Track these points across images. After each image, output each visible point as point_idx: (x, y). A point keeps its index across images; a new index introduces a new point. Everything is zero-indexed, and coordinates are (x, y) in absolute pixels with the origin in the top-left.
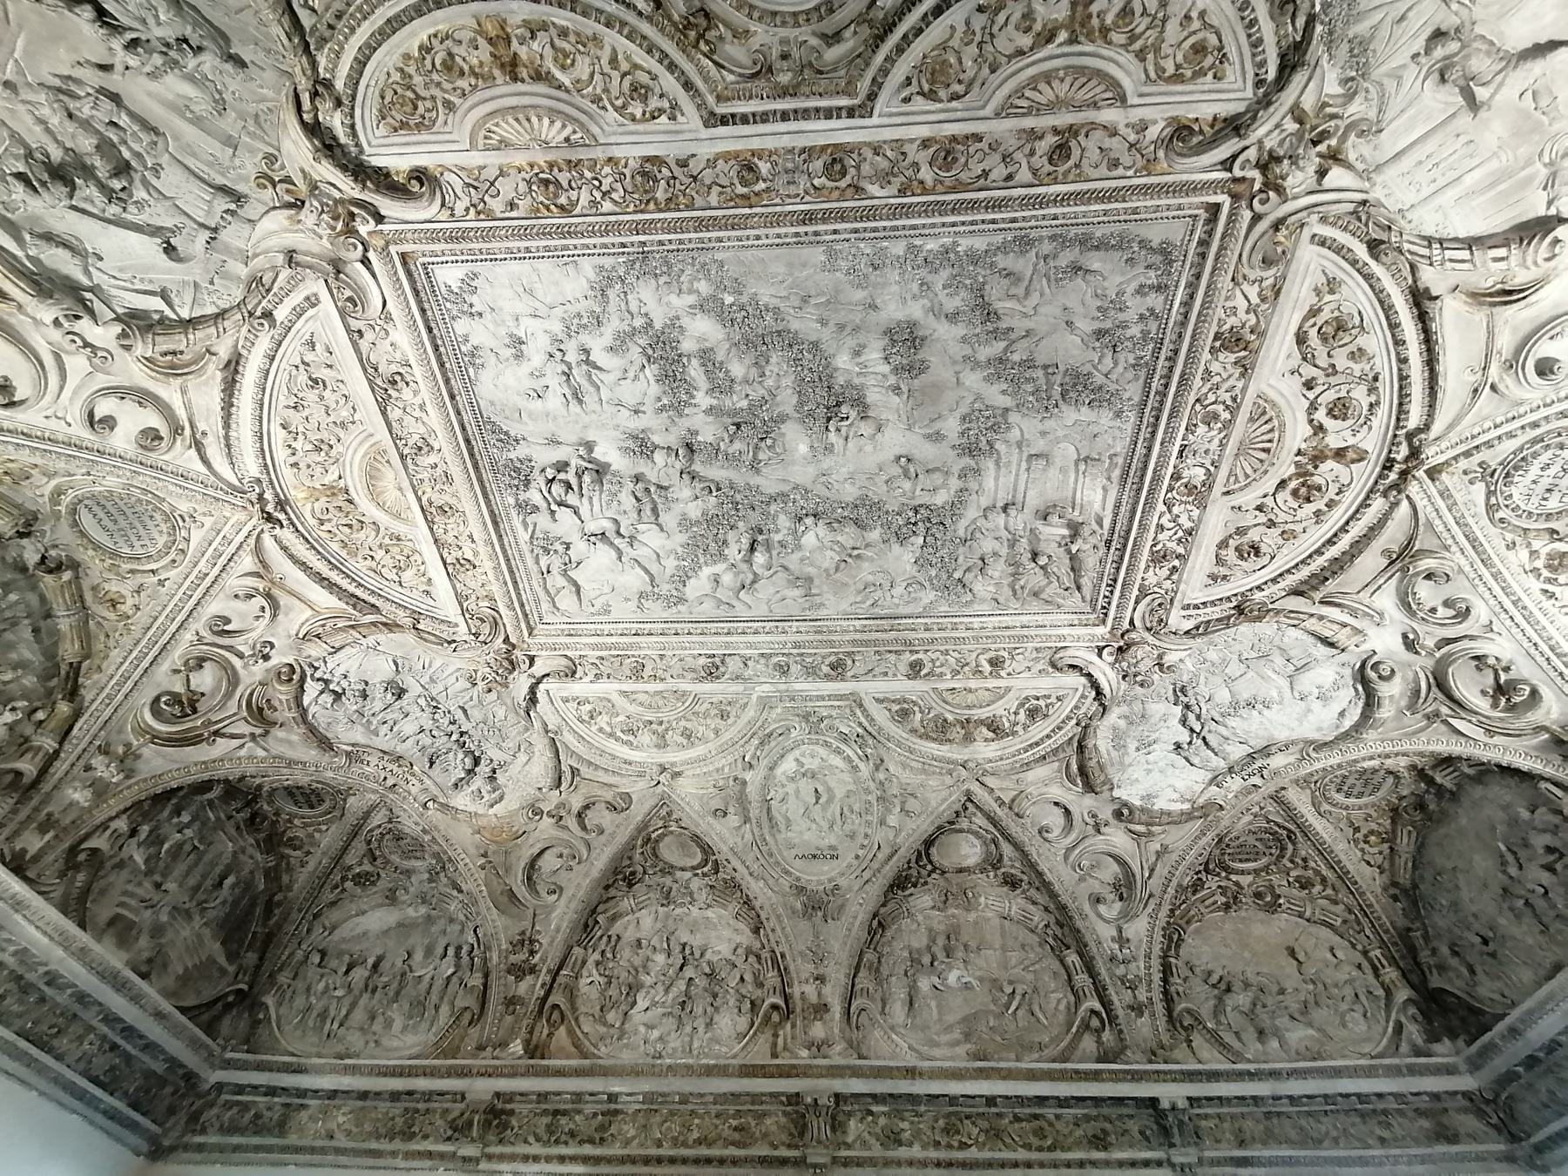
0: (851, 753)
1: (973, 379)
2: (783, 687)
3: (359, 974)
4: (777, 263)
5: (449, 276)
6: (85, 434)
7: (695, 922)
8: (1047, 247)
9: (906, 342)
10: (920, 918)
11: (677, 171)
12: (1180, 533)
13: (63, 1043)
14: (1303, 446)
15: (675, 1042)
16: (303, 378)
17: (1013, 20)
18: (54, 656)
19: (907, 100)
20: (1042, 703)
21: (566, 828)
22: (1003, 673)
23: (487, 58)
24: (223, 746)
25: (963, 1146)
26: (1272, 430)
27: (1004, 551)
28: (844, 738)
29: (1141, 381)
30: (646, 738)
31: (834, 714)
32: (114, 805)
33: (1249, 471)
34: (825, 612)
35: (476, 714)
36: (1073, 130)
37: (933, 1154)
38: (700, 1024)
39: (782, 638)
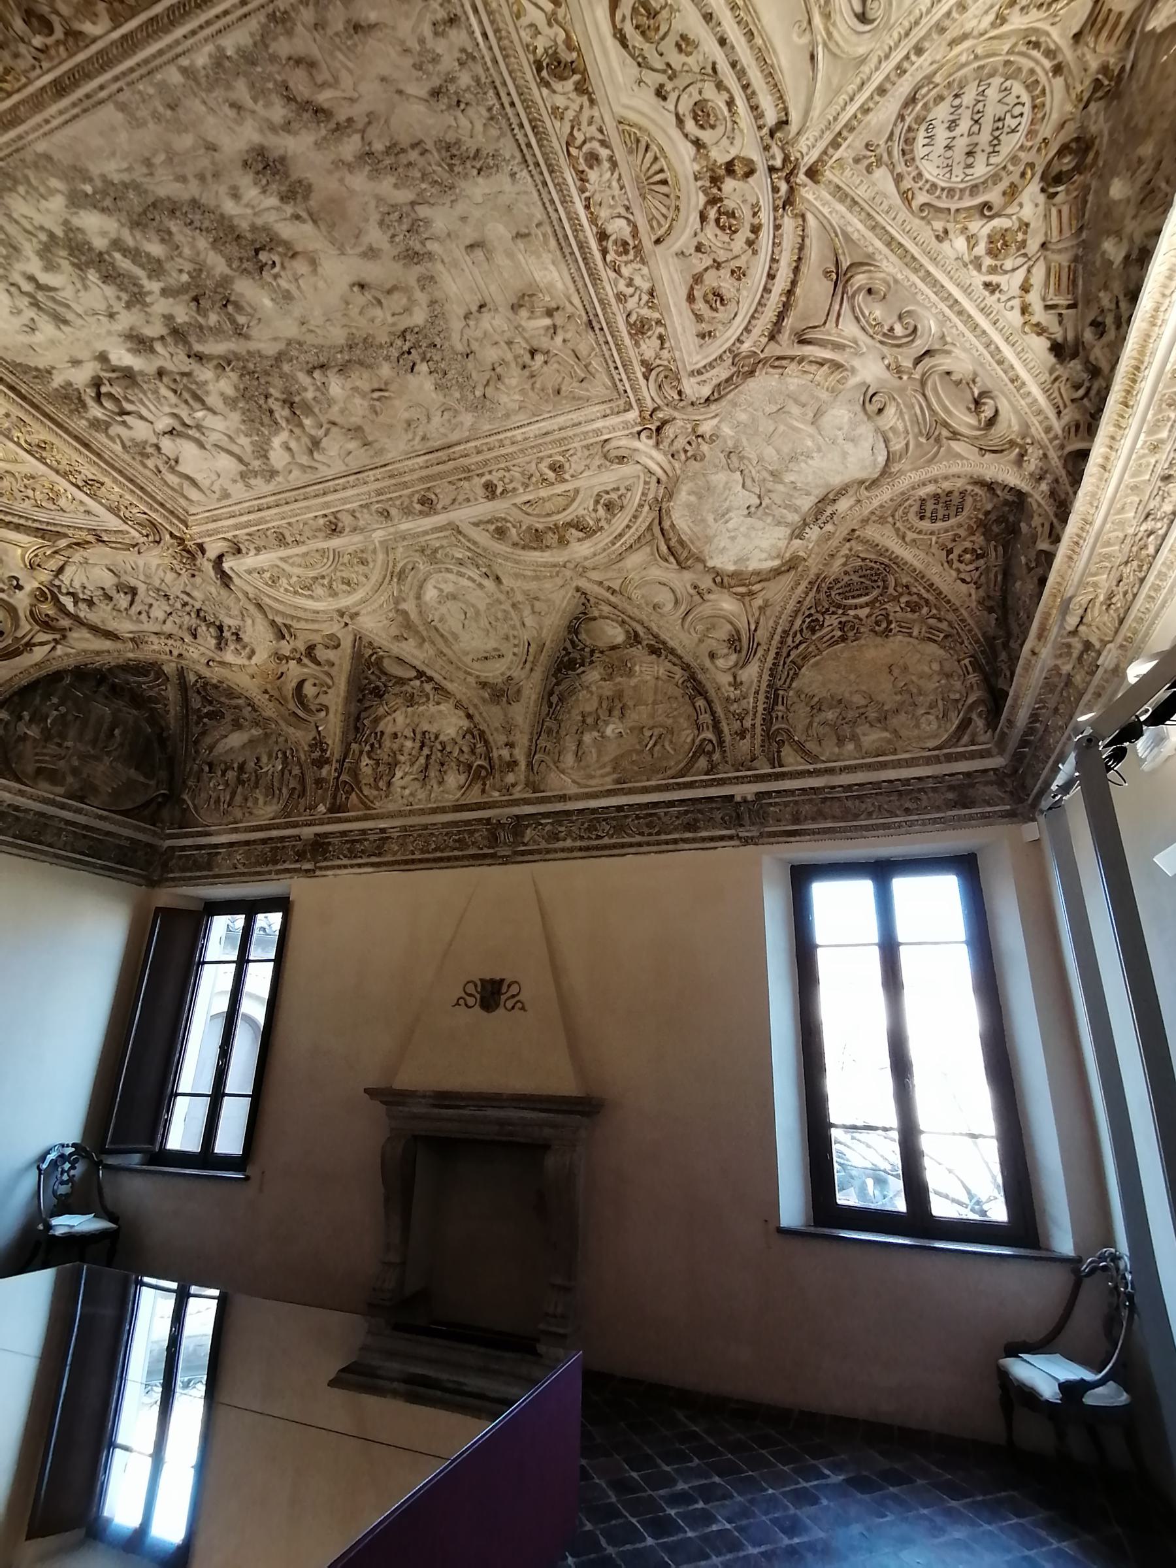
2: (392, 530)
3: (231, 775)
7: (432, 716)
9: (266, 165)
10: (594, 689)
13: (48, 838)
15: (421, 795)
20: (614, 496)
22: (567, 476)
24: (39, 653)
25: (599, 837)
26: (656, 159)
30: (319, 591)
31: (445, 542)
33: (664, 211)
34: (390, 456)
37: (578, 844)
38: (434, 782)
39: (365, 489)
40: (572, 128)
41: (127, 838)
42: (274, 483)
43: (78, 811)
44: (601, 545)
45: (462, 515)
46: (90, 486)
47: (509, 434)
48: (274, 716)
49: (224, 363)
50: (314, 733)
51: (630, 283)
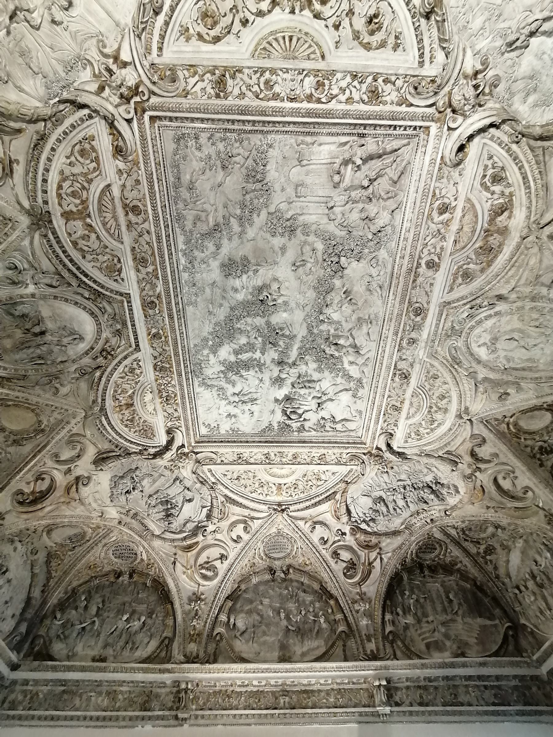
0: (485, 314)
1: (251, 233)
2: (423, 344)
4: (193, 325)
5: (204, 431)
6: (240, 546)
8: (181, 205)
9: (231, 267)
11: (158, 360)
12: (356, 83)
14: (288, 10)
16: (236, 481)
17: (86, 243)
18: (316, 591)
19: (123, 280)
20: (490, 172)
21: (486, 469)
22: (453, 204)
23: (127, 411)
26: (276, 39)
27: (360, 206)
28: (471, 316)
29: (249, 136)
30: (439, 416)
32: (378, 614)
33: (307, 45)
34: (381, 313)
35: (403, 477)
36: (125, 206)
39: (390, 339)
40: (250, 90)
41: (515, 677)
42: (365, 385)
43: (464, 665)
44: (524, 198)
45: (438, 295)
46: (322, 460)
47: (403, 232)
48: (509, 521)
49: (301, 357)
50: (541, 513)
51: (343, 90)
